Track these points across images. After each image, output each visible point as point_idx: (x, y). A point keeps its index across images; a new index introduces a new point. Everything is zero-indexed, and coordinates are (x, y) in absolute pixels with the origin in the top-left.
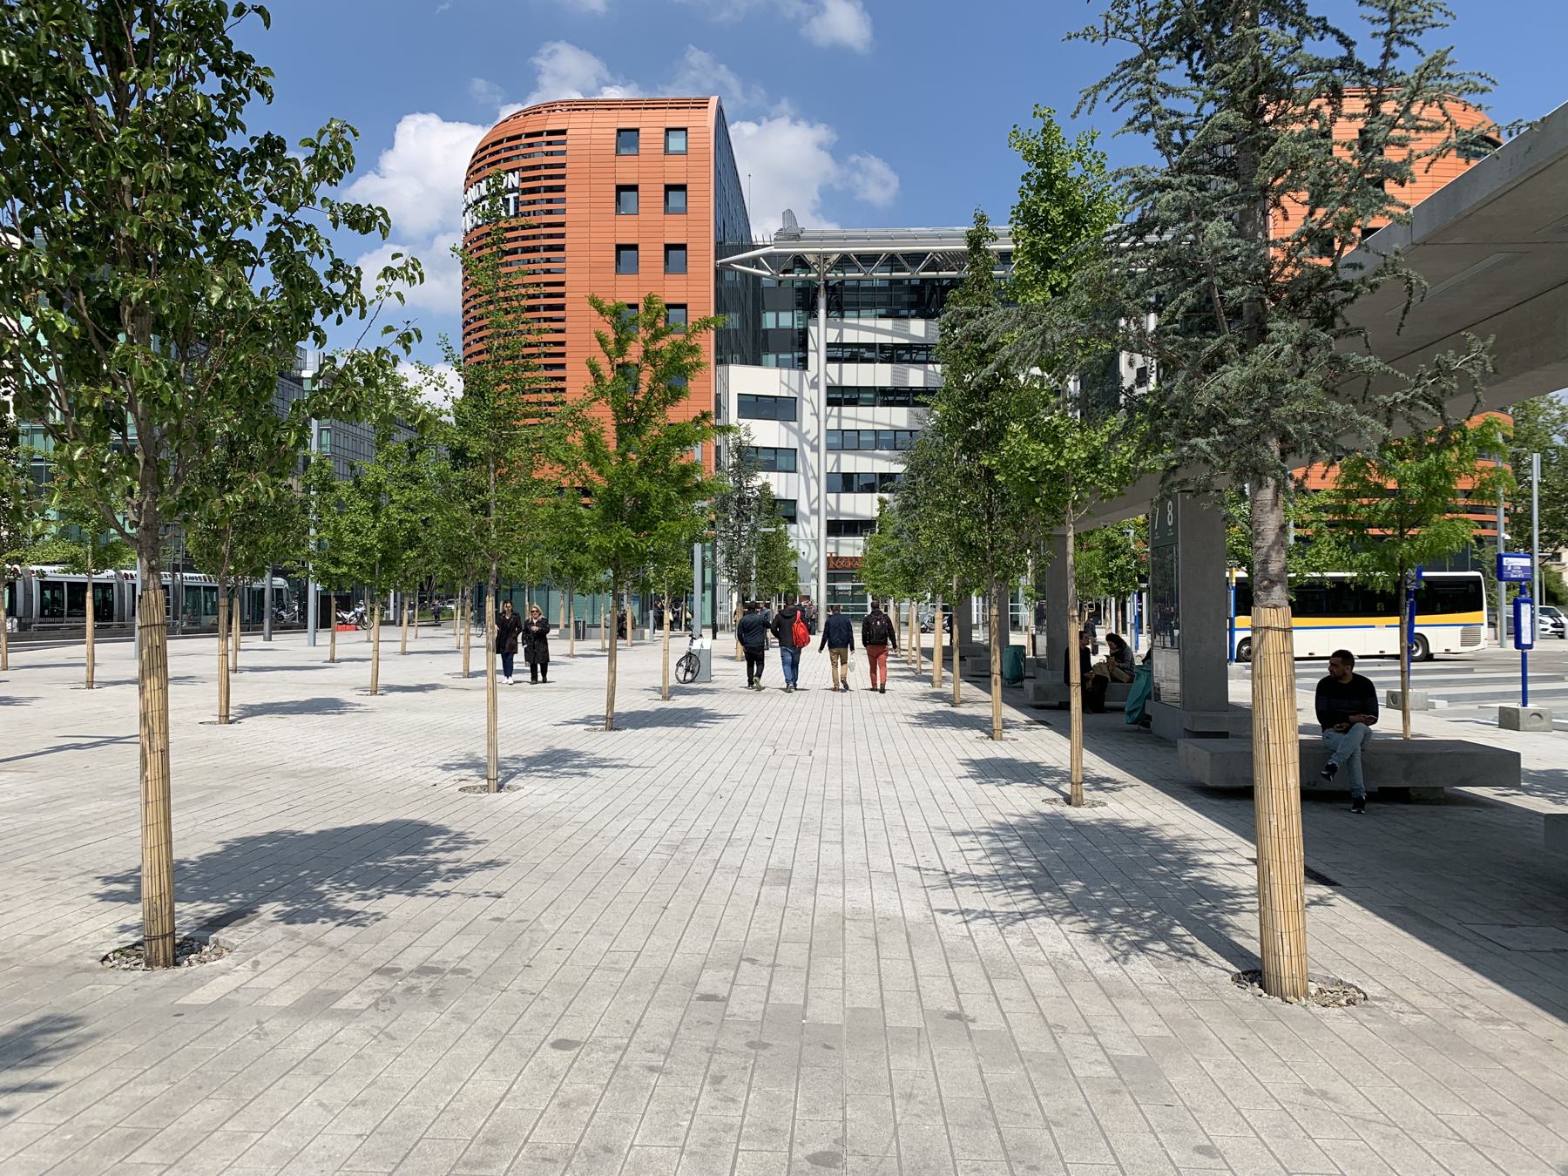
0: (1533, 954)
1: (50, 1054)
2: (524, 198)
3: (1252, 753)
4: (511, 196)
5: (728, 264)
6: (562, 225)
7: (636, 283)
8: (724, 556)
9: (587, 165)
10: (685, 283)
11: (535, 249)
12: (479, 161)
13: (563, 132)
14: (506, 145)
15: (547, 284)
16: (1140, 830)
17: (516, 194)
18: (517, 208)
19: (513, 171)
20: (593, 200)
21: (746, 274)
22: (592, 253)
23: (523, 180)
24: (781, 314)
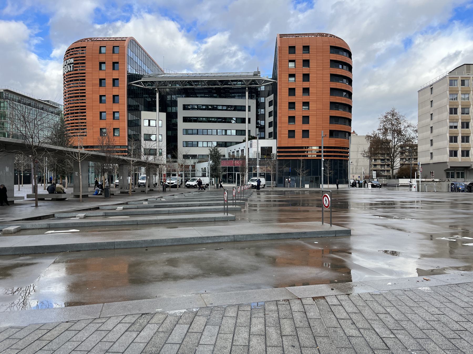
0: (95, 321)
1: (270, 238)
2: (75, 66)
3: (247, 235)
4: (71, 65)
5: (131, 84)
6: (84, 73)
7: (105, 89)
8: (94, 174)
9: (91, 57)
10: (118, 89)
11: (78, 80)
12: (68, 53)
13: (85, 47)
14: (75, 50)
15: (81, 90)
16: (173, 259)
17: (73, 65)
18: (73, 68)
19: (72, 58)
20: (93, 66)
21: (138, 87)
22: (93, 81)
23: (74, 61)
24: (257, 71)
